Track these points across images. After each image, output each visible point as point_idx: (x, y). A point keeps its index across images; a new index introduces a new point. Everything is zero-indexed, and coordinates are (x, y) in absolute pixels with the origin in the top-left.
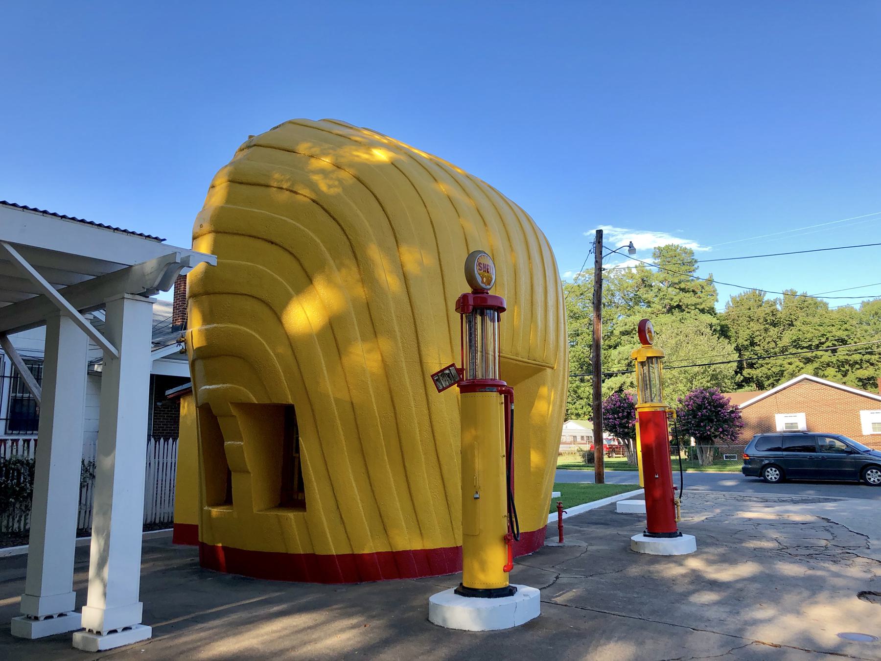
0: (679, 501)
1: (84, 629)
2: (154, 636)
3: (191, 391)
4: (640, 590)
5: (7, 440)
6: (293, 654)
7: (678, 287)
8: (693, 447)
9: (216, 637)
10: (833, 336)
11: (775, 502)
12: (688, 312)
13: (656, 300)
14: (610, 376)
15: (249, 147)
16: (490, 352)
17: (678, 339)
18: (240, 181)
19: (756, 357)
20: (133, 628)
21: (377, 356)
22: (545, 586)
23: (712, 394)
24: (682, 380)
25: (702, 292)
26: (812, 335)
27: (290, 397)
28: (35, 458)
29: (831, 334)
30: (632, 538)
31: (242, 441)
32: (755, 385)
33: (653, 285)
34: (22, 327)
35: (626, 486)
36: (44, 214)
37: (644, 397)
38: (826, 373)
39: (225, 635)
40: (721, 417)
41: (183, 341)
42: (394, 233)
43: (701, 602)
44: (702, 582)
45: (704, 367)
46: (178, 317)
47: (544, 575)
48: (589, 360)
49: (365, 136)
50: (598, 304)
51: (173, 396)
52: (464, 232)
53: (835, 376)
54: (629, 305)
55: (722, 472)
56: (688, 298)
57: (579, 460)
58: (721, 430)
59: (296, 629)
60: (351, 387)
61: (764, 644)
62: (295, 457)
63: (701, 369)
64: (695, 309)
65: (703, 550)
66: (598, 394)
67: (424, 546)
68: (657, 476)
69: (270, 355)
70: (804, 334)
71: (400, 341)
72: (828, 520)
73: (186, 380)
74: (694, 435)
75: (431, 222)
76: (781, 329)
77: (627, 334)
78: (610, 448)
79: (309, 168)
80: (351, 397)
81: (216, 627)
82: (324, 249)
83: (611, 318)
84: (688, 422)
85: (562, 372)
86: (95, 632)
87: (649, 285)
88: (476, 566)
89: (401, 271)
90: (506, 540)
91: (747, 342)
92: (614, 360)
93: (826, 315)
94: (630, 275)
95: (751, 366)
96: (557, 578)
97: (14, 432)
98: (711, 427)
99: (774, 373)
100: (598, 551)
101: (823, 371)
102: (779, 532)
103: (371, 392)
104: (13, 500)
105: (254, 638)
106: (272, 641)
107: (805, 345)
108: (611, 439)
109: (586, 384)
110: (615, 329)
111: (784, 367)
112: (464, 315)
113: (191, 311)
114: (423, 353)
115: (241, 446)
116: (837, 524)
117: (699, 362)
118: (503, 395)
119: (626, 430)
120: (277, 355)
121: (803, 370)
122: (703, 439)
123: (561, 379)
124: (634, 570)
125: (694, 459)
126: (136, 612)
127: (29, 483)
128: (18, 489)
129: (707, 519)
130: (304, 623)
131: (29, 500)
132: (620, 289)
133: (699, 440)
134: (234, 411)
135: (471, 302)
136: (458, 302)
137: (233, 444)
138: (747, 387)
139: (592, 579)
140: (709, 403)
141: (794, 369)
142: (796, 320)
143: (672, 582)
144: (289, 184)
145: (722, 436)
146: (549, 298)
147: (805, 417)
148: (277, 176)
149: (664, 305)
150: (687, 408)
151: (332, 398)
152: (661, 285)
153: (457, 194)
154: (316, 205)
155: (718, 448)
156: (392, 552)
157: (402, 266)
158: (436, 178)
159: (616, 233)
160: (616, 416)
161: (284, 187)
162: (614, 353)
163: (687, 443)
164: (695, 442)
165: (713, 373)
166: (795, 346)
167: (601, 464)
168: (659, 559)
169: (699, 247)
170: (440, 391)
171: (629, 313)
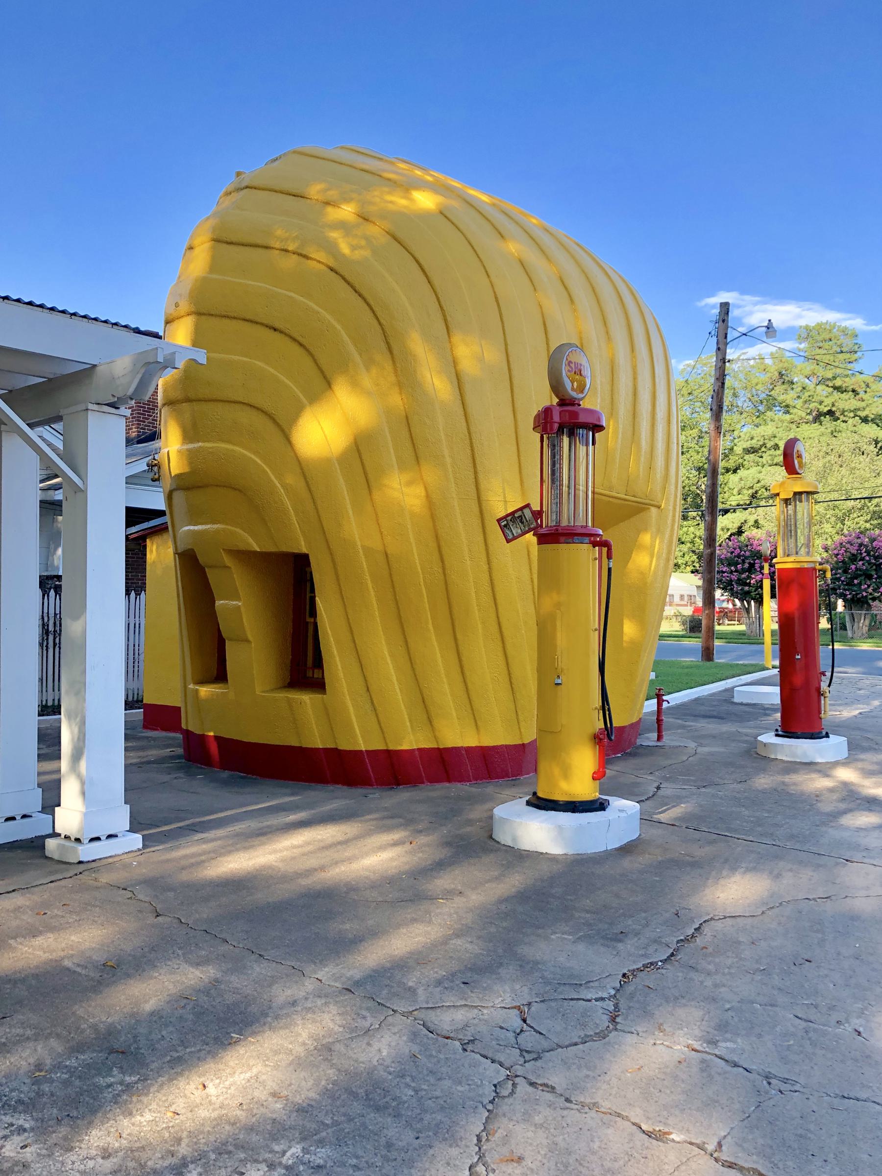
0: (827, 691)
1: (59, 835)
3: (167, 528)
6: (323, 875)
7: (831, 384)
8: (841, 613)
9: (223, 851)
12: (844, 421)
14: (726, 512)
16: (581, 488)
18: (228, 240)
21: (419, 491)
22: (643, 799)
23: (873, 540)
25: (866, 392)
30: (759, 738)
33: (795, 381)
35: (745, 665)
37: (786, 547)
39: (233, 849)
41: (156, 465)
42: (444, 316)
45: (863, 501)
46: (132, 425)
48: (697, 488)
49: (400, 171)
50: (717, 411)
51: (136, 535)
56: (846, 400)
59: (322, 844)
60: (385, 533)
66: (711, 539)
68: (799, 657)
73: (160, 513)
74: (843, 596)
75: (496, 298)
77: (753, 452)
78: (721, 612)
81: (219, 839)
82: (346, 338)
83: (731, 429)
86: (73, 839)
87: (789, 381)
88: (556, 771)
89: (453, 370)
92: (730, 496)
94: (762, 367)
96: (658, 788)
98: (869, 586)
100: (711, 754)
103: (412, 540)
105: (270, 853)
106: (293, 858)
108: (723, 601)
109: (690, 522)
113: (166, 422)
114: (482, 486)
115: (239, 607)
117: (856, 494)
118: (597, 548)
119: (747, 588)
122: (857, 602)
123: (669, 522)
124: (762, 781)
126: (121, 818)
129: (860, 713)
130: (333, 836)
132: (746, 387)
133: (849, 604)
134: (227, 560)
135: (556, 418)
136: (537, 417)
137: (226, 604)
143: (816, 798)
148: (279, 232)
149: (809, 411)
150: (835, 559)
151: (360, 547)
152: (807, 381)
154: (335, 275)
156: (438, 749)
157: (455, 363)
161: (290, 248)
162: (733, 479)
163: (831, 607)
165: (875, 509)
167: (711, 634)
168: (797, 766)
169: (865, 324)
170: (508, 541)
171: (757, 421)
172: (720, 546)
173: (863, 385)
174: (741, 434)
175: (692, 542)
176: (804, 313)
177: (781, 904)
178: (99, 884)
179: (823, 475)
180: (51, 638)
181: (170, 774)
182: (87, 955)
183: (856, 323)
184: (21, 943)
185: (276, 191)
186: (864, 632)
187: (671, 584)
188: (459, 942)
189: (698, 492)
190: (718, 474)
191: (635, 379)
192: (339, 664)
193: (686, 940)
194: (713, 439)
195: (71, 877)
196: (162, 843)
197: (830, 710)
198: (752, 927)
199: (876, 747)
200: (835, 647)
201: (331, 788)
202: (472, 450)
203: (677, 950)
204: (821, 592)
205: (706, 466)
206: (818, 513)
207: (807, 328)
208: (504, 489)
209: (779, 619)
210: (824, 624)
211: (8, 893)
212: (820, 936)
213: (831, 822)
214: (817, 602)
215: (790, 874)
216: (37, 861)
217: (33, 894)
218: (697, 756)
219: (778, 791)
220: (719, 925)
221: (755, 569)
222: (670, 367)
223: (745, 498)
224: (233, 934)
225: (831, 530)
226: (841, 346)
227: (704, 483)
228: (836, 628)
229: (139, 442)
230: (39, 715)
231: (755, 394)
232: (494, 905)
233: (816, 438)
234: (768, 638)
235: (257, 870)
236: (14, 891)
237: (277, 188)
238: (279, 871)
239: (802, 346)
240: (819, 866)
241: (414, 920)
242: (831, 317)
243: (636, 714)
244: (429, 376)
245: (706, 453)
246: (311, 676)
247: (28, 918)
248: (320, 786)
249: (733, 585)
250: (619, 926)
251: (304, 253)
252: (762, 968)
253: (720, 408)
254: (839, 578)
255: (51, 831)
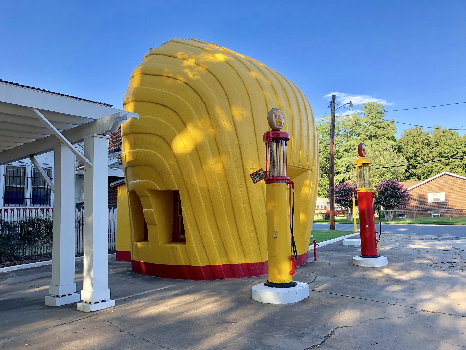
1: (83, 301)
2: (116, 305)
3: (125, 183)
4: (359, 284)
5: (32, 209)
6: (186, 314)
7: (374, 125)
8: (382, 211)
9: (147, 306)
10: (461, 151)
11: (428, 239)
12: (380, 139)
13: (363, 132)
14: (337, 174)
15: (151, 55)
16: (282, 163)
17: (374, 153)
19: (417, 162)
20: (106, 301)
21: (220, 165)
23: (393, 183)
24: (376, 175)
26: (449, 150)
27: (176, 186)
28: (47, 218)
29: (460, 150)
31: (153, 209)
32: (416, 178)
33: (361, 124)
34: (42, 151)
36: (53, 94)
37: (361, 185)
38: (457, 171)
40: (398, 195)
41: (120, 158)
43: (392, 290)
44: (392, 280)
45: (389, 168)
47: (308, 276)
49: (211, 47)
50: (332, 136)
51: (113, 186)
52: (265, 98)
53: (462, 172)
54: (348, 135)
55: (398, 224)
56: (381, 131)
57: (320, 218)
58: (398, 202)
59: (186, 303)
61: (427, 311)
62: (179, 217)
63: (387, 170)
64: (384, 137)
65: (391, 264)
66: (332, 184)
67: (246, 262)
68: (367, 226)
69: (166, 165)
70: (445, 150)
71: (232, 157)
72: (458, 249)
73: (122, 178)
74: (383, 204)
75: (248, 93)
76: (431, 147)
77: (347, 151)
79: (182, 65)
80: (207, 186)
81: (146, 301)
82: (191, 109)
83: (338, 143)
84: (380, 198)
85: (316, 172)
87: (359, 124)
88: (276, 272)
90: (291, 258)
92: (340, 165)
93: (458, 139)
94: (349, 119)
95: (414, 167)
96: (315, 278)
97: (34, 205)
98: (392, 201)
99: (427, 171)
100: (335, 265)
101: (455, 170)
102: (432, 255)
104: (37, 239)
106: (174, 308)
107: (445, 156)
108: (338, 207)
109: (324, 178)
110: (340, 149)
111: (433, 168)
112: (267, 143)
113: (124, 142)
116: (463, 251)
117: (386, 166)
118: (288, 185)
119: (346, 202)
120: (169, 165)
121: (443, 170)
122: (388, 207)
123: (316, 176)
124: (355, 274)
125: (383, 217)
126: (107, 294)
127: (45, 230)
128: (39, 233)
130: (189, 299)
131: (45, 239)
132: (343, 127)
133: (385, 207)
134: (148, 194)
136: (264, 136)
138: (412, 179)
139: (334, 278)
140: (392, 188)
141: (439, 169)
142: (440, 142)
144: (172, 75)
145: (398, 205)
146: (310, 133)
148: (166, 70)
150: (379, 190)
153: (260, 77)
155: (396, 212)
156: (230, 265)
157: (233, 117)
158: (250, 70)
159: (341, 96)
160: (341, 195)
162: (339, 161)
163: (379, 209)
164: (384, 208)
166: (439, 157)
167: (334, 220)
168: (369, 269)
169: (387, 103)
170: (255, 183)
171: (347, 140)
172: (336, 186)
173: (387, 125)
174: (342, 145)
175: (325, 186)
176: (364, 99)
177: (364, 321)
178: (98, 320)
179: (374, 158)
180: (81, 226)
181: (126, 277)
182: (93, 348)
183: (383, 102)
184: (67, 344)
185: (164, 55)
186: (392, 218)
187: (317, 202)
188: (239, 339)
189: (327, 167)
190: (333, 160)
191: (301, 122)
192: (191, 232)
193: (328, 336)
194: (331, 146)
195: (87, 318)
196: (123, 303)
197: (380, 247)
198: (354, 330)
199: (398, 260)
200: (381, 224)
201: (189, 281)
202: (240, 149)
203: (325, 340)
204: (375, 203)
205: (329, 157)
206: (372, 173)
207: (365, 104)
208: (252, 164)
209: (359, 212)
210: (376, 215)
211: (62, 324)
212: (381, 333)
213: (383, 289)
214: (373, 207)
215: (368, 309)
216: (74, 312)
217: (72, 325)
218: (330, 266)
219: (361, 278)
220: (341, 330)
221: (349, 195)
222: (314, 120)
223: (344, 169)
224: (150, 338)
225: (377, 180)
226: (378, 111)
227: (328, 163)
228: (381, 217)
229: (115, 152)
230: (75, 256)
231: (346, 129)
232: (252, 324)
233: (370, 145)
234: (355, 221)
235: (160, 313)
236: (64, 324)
237: (165, 54)
238: (169, 313)
239: (363, 111)
240: (379, 306)
241: (222, 331)
242: (374, 100)
243: (306, 250)
244: (223, 122)
245: (329, 152)
246: (180, 238)
247: (69, 334)
248: (184, 281)
249: (341, 201)
250: (302, 331)
251: (175, 77)
252: (358, 346)
253: (333, 134)
254: (381, 198)
255: (80, 300)
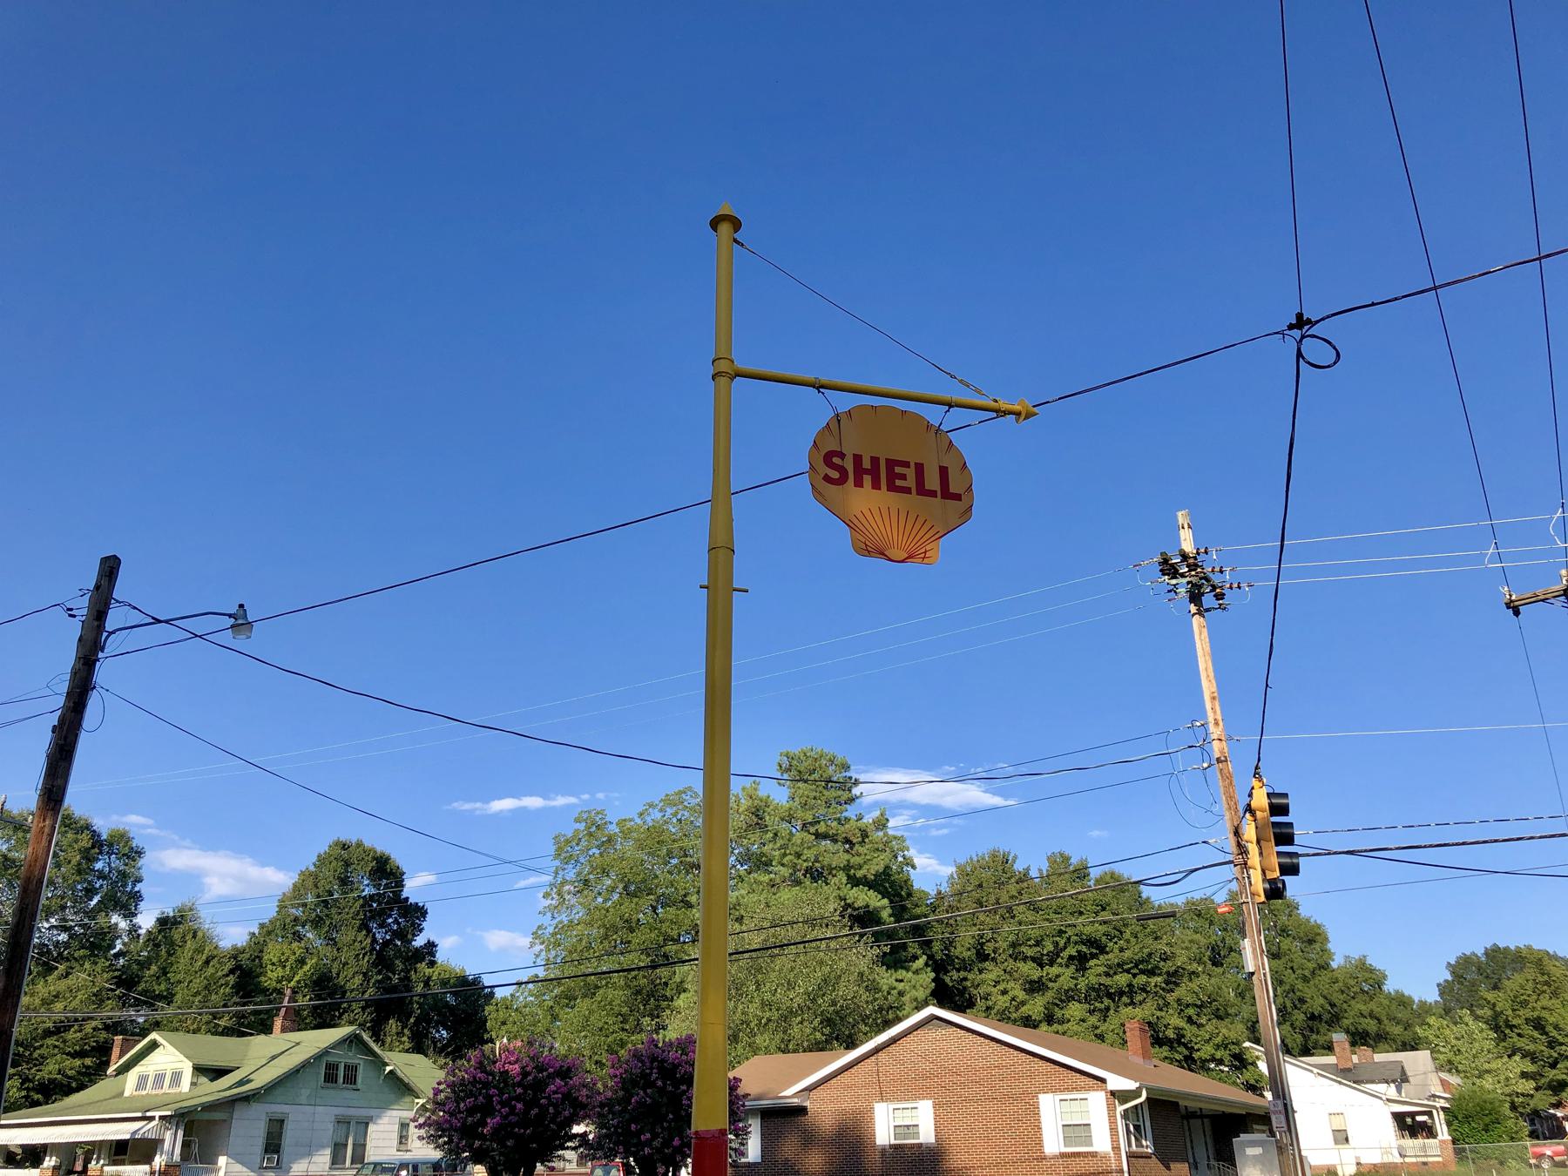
91: (969, 953)
147: (932, 1111)
